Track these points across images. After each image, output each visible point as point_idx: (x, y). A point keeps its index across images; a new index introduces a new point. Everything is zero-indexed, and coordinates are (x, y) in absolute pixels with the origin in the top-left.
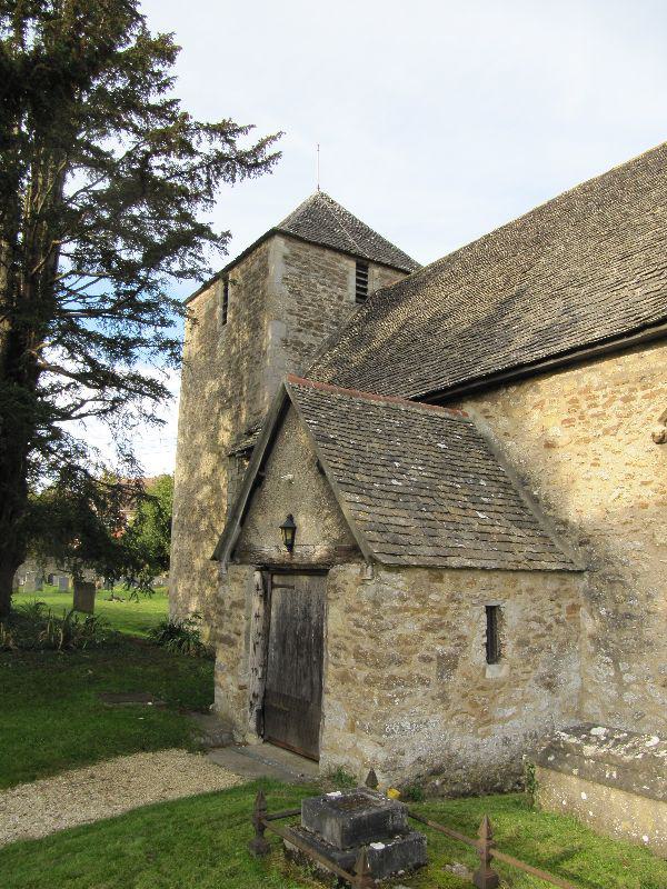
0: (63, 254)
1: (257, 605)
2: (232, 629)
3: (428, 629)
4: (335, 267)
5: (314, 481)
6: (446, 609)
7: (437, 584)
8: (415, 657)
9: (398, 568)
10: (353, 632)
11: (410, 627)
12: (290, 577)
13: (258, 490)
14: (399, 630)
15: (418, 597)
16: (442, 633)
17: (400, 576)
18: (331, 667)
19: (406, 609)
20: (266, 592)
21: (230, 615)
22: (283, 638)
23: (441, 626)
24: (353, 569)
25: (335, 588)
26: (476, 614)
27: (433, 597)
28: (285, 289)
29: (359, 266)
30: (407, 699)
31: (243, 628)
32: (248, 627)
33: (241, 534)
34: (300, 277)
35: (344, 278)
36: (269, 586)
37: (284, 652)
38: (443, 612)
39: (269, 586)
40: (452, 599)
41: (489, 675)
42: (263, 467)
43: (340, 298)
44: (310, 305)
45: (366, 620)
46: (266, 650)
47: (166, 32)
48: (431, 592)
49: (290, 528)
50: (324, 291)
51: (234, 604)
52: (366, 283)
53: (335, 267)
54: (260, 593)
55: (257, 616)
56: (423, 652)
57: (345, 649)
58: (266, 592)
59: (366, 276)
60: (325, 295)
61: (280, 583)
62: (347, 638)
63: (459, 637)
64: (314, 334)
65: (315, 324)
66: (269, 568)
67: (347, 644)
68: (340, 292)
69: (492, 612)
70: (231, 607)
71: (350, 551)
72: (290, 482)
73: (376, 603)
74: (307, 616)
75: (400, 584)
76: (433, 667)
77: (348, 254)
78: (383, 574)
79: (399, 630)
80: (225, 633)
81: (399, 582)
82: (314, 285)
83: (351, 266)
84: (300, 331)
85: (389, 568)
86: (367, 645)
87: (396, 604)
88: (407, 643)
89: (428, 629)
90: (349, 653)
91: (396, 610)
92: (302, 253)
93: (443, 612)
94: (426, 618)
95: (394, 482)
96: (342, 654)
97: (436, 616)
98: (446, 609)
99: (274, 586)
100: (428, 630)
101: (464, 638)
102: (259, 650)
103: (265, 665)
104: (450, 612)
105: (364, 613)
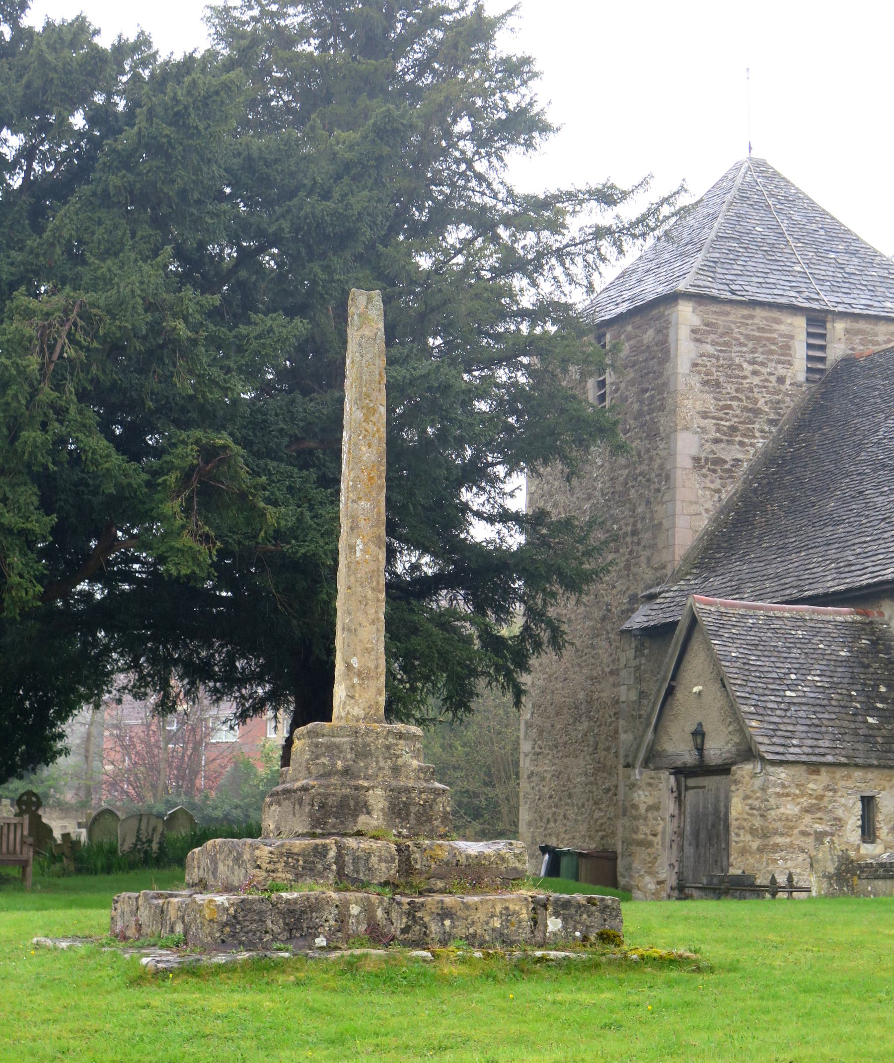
0: (700, 750)
1: (671, 807)
2: (648, 832)
3: (807, 811)
4: (771, 331)
5: (719, 694)
6: (823, 796)
7: (815, 777)
8: (796, 831)
9: (781, 763)
10: (748, 814)
11: (790, 809)
12: (701, 779)
13: (670, 698)
14: (782, 810)
15: (798, 786)
16: (819, 815)
17: (781, 769)
18: (734, 844)
19: (787, 795)
20: (680, 794)
21: (646, 819)
22: (696, 834)
23: (820, 809)
24: (748, 767)
25: (736, 782)
26: (851, 801)
27: (811, 786)
28: (695, 381)
29: (810, 322)
30: (789, 862)
31: (659, 829)
32: (664, 828)
33: (654, 741)
34: (718, 359)
35: (786, 349)
36: (683, 788)
37: (697, 846)
38: (821, 798)
39: (683, 788)
40: (827, 788)
41: (863, 851)
42: (674, 678)
43: (781, 380)
44: (732, 399)
45: (757, 803)
46: (681, 849)
47: (550, 118)
48: (809, 783)
49: (699, 734)
50: (755, 373)
51: (650, 808)
52: (823, 348)
53: (771, 331)
54: (675, 794)
55: (673, 816)
56: (802, 828)
57: (743, 828)
58: (680, 794)
59: (823, 336)
60: (756, 380)
61: (693, 785)
62: (745, 820)
63: (835, 819)
64: (741, 444)
65: (741, 427)
66: (681, 772)
67: (745, 824)
68: (781, 371)
69: (868, 802)
70: (647, 811)
71: (748, 753)
72: (700, 693)
73: (764, 789)
74: (717, 811)
75: (783, 776)
76: (811, 839)
77: (794, 309)
78: (771, 769)
79: (782, 810)
80: (641, 837)
81: (782, 774)
82: (740, 366)
83: (800, 322)
84: (717, 441)
85: (773, 763)
86: (758, 822)
87: (778, 790)
88: (787, 819)
89: (807, 811)
90: (746, 831)
91: (778, 795)
92: (721, 321)
93: (821, 798)
94: (805, 802)
95: (788, 693)
96: (742, 832)
97: (814, 801)
98: (823, 796)
99: (687, 788)
100: (807, 811)
101: (840, 820)
102: (675, 846)
103: (681, 861)
104: (826, 799)
105: (757, 799)
